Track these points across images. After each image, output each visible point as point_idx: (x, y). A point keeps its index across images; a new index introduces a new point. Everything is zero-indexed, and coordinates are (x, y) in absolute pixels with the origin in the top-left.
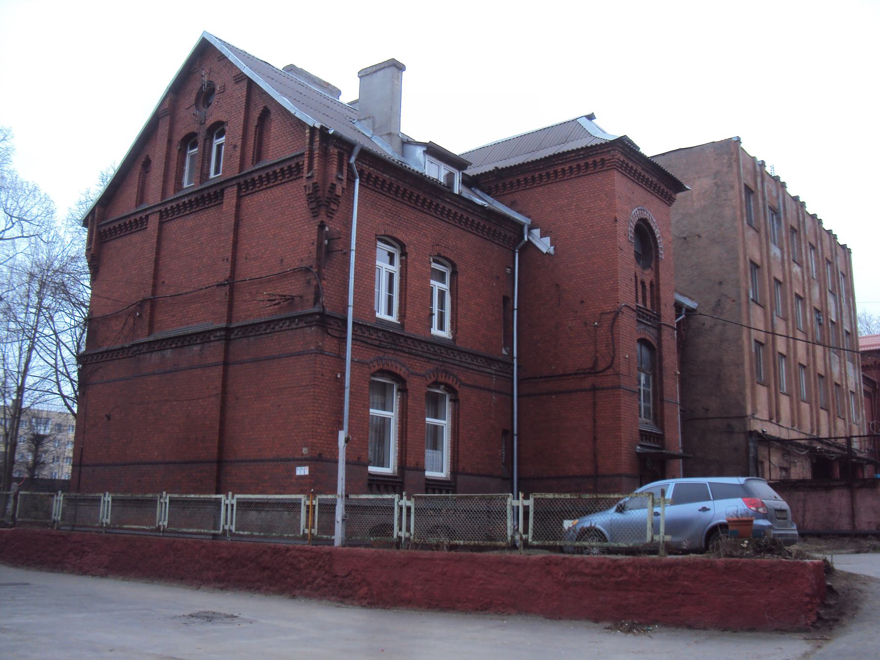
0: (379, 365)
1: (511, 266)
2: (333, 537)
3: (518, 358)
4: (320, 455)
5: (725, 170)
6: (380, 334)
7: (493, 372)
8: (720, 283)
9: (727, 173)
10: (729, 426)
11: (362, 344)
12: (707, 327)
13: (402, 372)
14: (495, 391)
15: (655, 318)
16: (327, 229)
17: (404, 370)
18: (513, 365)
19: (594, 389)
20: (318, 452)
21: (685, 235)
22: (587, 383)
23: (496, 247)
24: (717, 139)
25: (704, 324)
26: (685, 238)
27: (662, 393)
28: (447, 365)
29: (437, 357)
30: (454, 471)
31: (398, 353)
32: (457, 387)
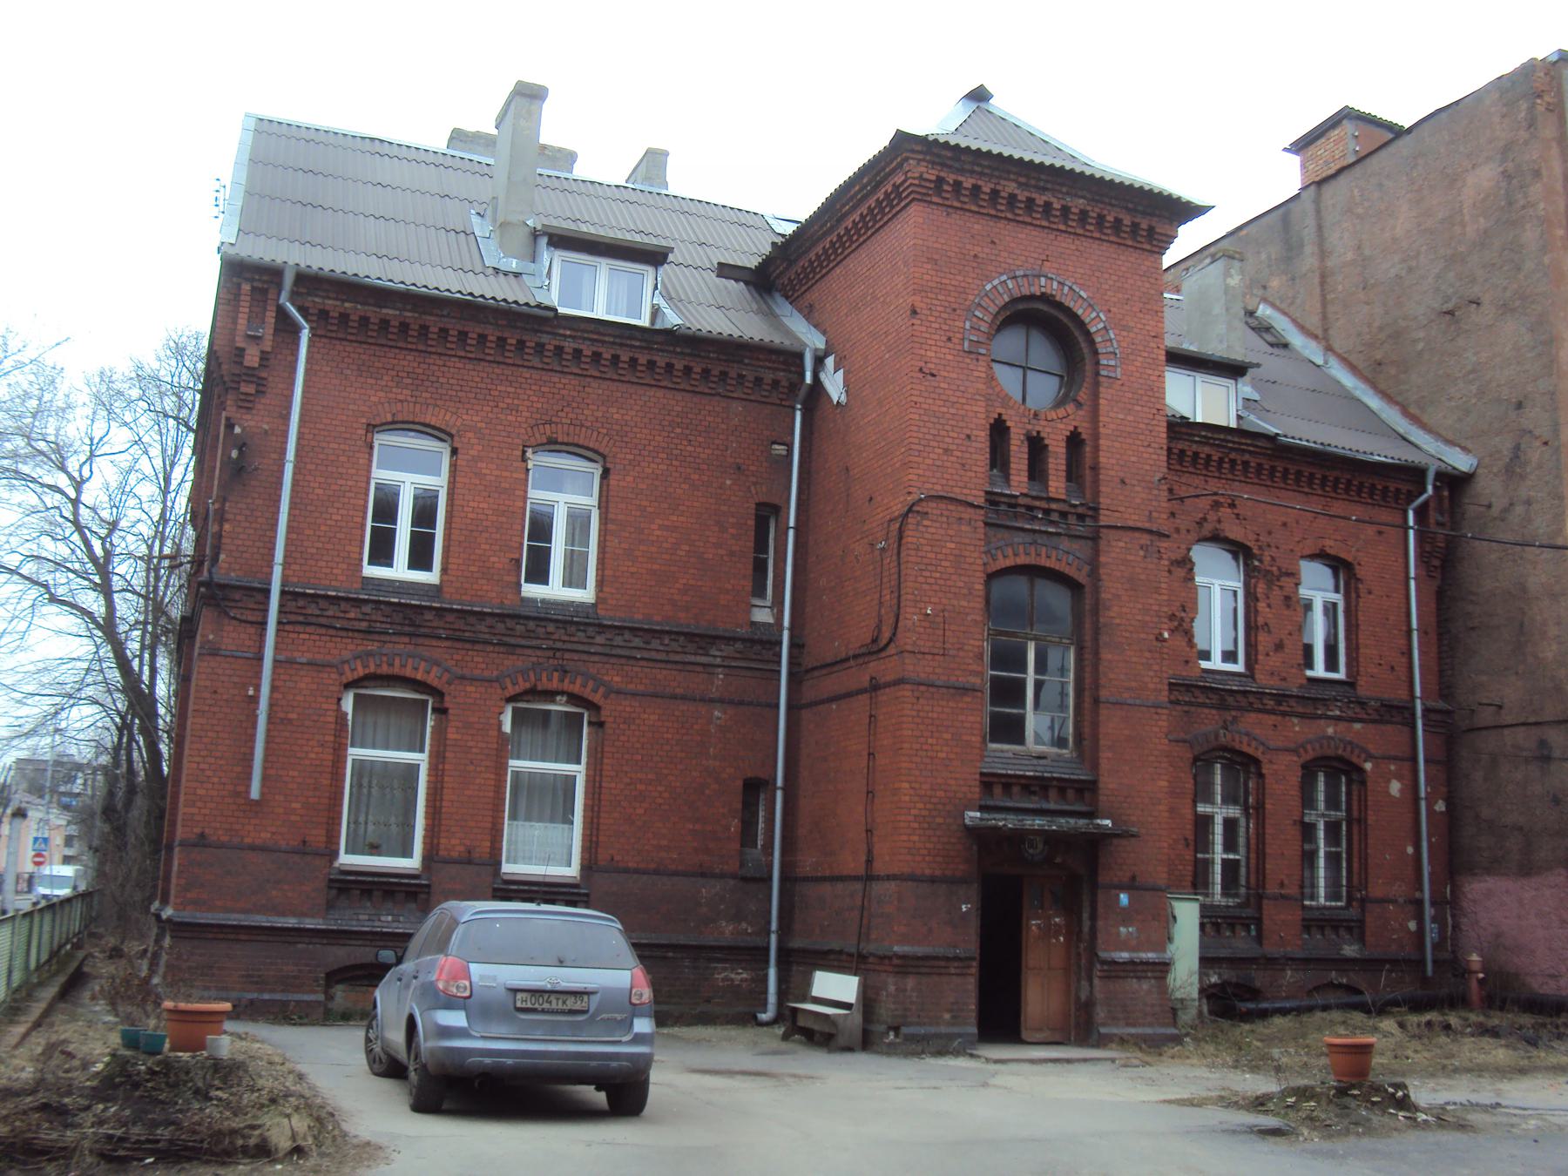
0: (365, 667)
1: (787, 439)
2: (1168, 954)
3: (791, 629)
4: (202, 835)
5: (1523, 135)
6: (367, 609)
7: (718, 661)
8: (1519, 405)
9: (1526, 143)
10: (1543, 743)
11: (323, 631)
12: (1495, 511)
13: (433, 678)
14: (722, 701)
15: (1081, 517)
16: (237, 430)
17: (435, 671)
18: (780, 643)
19: (875, 687)
20: (197, 830)
21: (1449, 306)
22: (860, 677)
23: (737, 407)
24: (1507, 68)
25: (1489, 506)
26: (1450, 313)
27: (1096, 686)
28: (567, 656)
29: (534, 643)
30: (588, 867)
31: (420, 640)
32: (597, 698)
